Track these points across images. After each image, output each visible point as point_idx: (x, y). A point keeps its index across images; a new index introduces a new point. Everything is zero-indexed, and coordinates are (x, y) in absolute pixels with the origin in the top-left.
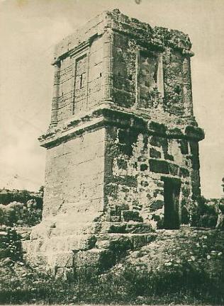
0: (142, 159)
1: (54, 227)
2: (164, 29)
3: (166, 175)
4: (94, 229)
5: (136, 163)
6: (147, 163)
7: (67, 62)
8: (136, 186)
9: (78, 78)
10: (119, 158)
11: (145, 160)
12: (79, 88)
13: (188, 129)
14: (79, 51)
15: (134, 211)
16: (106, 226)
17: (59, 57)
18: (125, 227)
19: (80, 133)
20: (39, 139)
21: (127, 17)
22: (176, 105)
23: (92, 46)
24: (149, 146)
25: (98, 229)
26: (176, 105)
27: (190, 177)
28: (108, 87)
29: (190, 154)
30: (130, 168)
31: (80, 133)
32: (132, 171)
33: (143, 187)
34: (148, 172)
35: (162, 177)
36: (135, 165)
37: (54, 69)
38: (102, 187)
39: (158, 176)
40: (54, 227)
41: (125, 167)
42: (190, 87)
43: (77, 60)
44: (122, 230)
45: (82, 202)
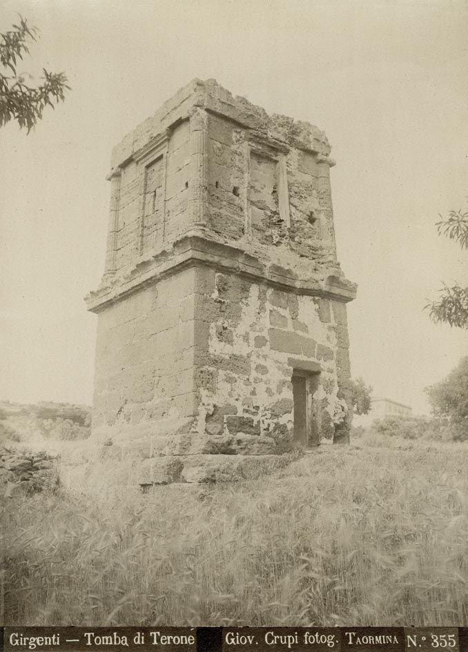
0: (258, 327)
1: (110, 444)
2: (288, 118)
3: (296, 357)
4: (178, 447)
5: (247, 334)
6: (265, 334)
7: (134, 172)
8: (246, 371)
9: (149, 197)
10: (219, 323)
11: (261, 330)
12: (151, 212)
13: (56, 419)
14: (145, 156)
15: (246, 415)
16: (199, 443)
17: (119, 167)
18: (229, 443)
19: (151, 283)
20: (85, 299)
21: (229, 93)
22: (309, 242)
23: (171, 143)
24: (268, 306)
25: (185, 447)
26: (309, 242)
27: (334, 361)
28: (199, 202)
29: (333, 323)
30: (238, 341)
31: (151, 283)
32: (240, 348)
33: (260, 376)
34: (266, 349)
35: (289, 359)
36: (246, 338)
37: (109, 187)
38: (191, 373)
39: (284, 357)
40: (110, 444)
41: (230, 342)
42: (330, 215)
43: (148, 167)
44: (226, 450)
45: (156, 401)
